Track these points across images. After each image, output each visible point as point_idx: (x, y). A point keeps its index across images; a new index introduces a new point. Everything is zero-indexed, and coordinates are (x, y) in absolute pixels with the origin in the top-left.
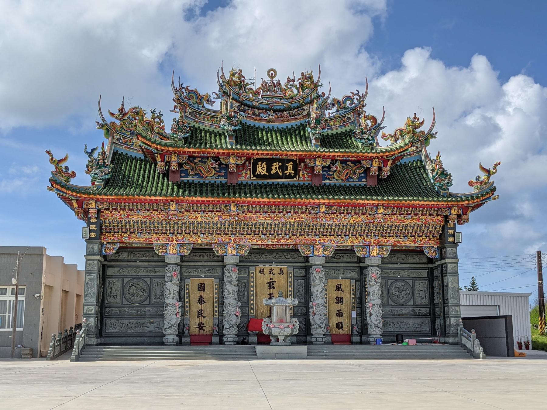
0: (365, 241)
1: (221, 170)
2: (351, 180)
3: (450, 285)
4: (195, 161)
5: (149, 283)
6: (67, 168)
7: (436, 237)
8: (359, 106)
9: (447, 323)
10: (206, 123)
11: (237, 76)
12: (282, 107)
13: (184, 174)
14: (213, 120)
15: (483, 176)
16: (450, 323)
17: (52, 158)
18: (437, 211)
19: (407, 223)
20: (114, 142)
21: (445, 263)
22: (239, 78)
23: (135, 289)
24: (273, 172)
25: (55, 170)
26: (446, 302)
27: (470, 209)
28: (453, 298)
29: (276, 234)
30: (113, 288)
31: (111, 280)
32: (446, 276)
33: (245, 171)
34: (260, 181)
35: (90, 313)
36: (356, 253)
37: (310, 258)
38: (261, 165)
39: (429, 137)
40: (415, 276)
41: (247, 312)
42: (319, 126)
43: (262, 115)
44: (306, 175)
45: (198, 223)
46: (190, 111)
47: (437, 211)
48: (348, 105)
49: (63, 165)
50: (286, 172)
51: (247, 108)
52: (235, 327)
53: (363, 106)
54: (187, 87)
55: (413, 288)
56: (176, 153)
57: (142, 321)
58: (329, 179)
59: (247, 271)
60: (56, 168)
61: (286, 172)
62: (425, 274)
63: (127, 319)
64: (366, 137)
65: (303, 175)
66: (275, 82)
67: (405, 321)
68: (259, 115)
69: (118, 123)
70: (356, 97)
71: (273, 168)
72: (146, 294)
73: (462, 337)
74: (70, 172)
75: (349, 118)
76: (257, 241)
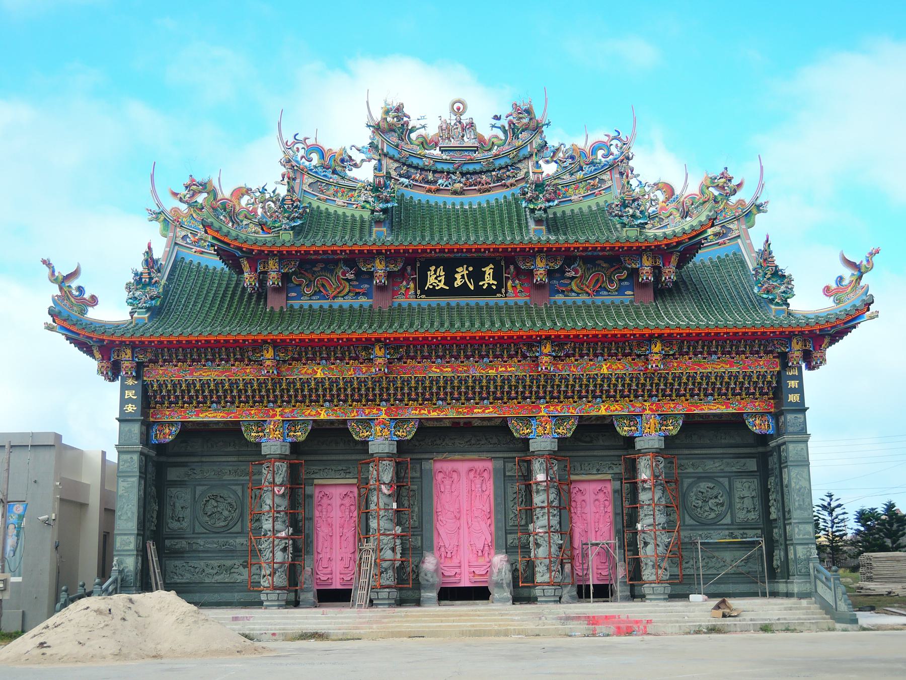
0: (633, 407)
1: (360, 284)
2: (605, 293)
3: (793, 485)
4: (315, 269)
5: (240, 494)
6: (80, 289)
7: (767, 394)
8: (621, 158)
9: (791, 556)
10: (340, 201)
11: (392, 114)
12: (478, 167)
13: (294, 294)
14: (352, 196)
15: (848, 274)
16: (795, 554)
17: (53, 272)
18: (765, 346)
19: (709, 370)
20: (176, 244)
21: (784, 443)
22: (399, 118)
23: (216, 504)
24: (458, 283)
25: (59, 294)
26: (787, 516)
27: (827, 340)
28: (800, 508)
29: (463, 398)
30: (177, 505)
31: (173, 491)
32: (786, 467)
33: (404, 283)
34: (434, 301)
35: (126, 548)
36: (618, 429)
37: (531, 441)
38: (435, 271)
39: (754, 211)
40: (734, 469)
41: (420, 544)
42: (541, 196)
43: (440, 181)
44: (518, 287)
45: (318, 382)
46: (311, 181)
47: (765, 346)
48: (599, 157)
49: (74, 284)
50: (481, 283)
51: (412, 170)
52: (390, 573)
53: (628, 159)
54: (306, 139)
55: (730, 493)
56: (275, 255)
57: (229, 563)
58: (563, 292)
59: (418, 469)
60: (61, 289)
61: (481, 283)
62: (752, 465)
63: (201, 559)
64: (631, 211)
65: (514, 287)
66: (464, 122)
67: (716, 554)
68: (436, 182)
69: (183, 207)
70: (614, 142)
71: (458, 276)
72: (236, 515)
73: (818, 582)
74: (87, 296)
75: (602, 181)
76: (429, 412)
